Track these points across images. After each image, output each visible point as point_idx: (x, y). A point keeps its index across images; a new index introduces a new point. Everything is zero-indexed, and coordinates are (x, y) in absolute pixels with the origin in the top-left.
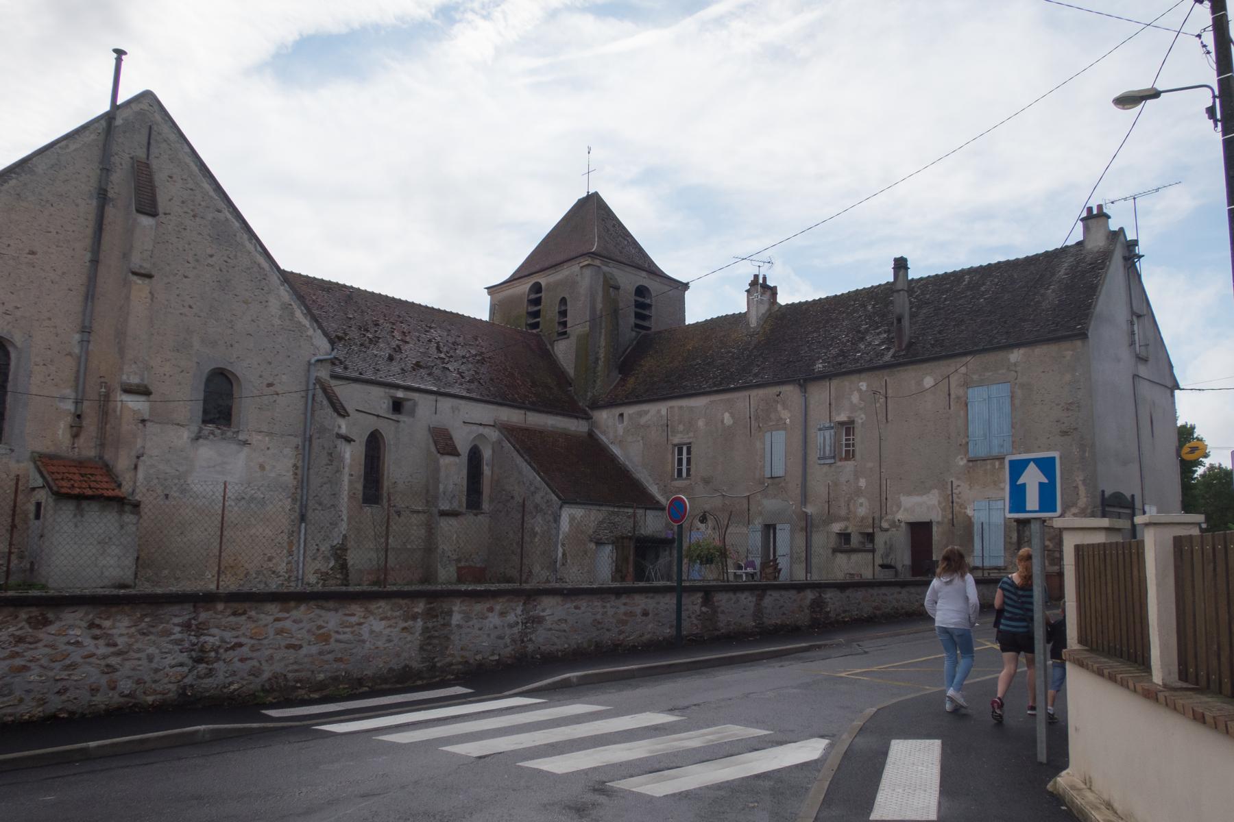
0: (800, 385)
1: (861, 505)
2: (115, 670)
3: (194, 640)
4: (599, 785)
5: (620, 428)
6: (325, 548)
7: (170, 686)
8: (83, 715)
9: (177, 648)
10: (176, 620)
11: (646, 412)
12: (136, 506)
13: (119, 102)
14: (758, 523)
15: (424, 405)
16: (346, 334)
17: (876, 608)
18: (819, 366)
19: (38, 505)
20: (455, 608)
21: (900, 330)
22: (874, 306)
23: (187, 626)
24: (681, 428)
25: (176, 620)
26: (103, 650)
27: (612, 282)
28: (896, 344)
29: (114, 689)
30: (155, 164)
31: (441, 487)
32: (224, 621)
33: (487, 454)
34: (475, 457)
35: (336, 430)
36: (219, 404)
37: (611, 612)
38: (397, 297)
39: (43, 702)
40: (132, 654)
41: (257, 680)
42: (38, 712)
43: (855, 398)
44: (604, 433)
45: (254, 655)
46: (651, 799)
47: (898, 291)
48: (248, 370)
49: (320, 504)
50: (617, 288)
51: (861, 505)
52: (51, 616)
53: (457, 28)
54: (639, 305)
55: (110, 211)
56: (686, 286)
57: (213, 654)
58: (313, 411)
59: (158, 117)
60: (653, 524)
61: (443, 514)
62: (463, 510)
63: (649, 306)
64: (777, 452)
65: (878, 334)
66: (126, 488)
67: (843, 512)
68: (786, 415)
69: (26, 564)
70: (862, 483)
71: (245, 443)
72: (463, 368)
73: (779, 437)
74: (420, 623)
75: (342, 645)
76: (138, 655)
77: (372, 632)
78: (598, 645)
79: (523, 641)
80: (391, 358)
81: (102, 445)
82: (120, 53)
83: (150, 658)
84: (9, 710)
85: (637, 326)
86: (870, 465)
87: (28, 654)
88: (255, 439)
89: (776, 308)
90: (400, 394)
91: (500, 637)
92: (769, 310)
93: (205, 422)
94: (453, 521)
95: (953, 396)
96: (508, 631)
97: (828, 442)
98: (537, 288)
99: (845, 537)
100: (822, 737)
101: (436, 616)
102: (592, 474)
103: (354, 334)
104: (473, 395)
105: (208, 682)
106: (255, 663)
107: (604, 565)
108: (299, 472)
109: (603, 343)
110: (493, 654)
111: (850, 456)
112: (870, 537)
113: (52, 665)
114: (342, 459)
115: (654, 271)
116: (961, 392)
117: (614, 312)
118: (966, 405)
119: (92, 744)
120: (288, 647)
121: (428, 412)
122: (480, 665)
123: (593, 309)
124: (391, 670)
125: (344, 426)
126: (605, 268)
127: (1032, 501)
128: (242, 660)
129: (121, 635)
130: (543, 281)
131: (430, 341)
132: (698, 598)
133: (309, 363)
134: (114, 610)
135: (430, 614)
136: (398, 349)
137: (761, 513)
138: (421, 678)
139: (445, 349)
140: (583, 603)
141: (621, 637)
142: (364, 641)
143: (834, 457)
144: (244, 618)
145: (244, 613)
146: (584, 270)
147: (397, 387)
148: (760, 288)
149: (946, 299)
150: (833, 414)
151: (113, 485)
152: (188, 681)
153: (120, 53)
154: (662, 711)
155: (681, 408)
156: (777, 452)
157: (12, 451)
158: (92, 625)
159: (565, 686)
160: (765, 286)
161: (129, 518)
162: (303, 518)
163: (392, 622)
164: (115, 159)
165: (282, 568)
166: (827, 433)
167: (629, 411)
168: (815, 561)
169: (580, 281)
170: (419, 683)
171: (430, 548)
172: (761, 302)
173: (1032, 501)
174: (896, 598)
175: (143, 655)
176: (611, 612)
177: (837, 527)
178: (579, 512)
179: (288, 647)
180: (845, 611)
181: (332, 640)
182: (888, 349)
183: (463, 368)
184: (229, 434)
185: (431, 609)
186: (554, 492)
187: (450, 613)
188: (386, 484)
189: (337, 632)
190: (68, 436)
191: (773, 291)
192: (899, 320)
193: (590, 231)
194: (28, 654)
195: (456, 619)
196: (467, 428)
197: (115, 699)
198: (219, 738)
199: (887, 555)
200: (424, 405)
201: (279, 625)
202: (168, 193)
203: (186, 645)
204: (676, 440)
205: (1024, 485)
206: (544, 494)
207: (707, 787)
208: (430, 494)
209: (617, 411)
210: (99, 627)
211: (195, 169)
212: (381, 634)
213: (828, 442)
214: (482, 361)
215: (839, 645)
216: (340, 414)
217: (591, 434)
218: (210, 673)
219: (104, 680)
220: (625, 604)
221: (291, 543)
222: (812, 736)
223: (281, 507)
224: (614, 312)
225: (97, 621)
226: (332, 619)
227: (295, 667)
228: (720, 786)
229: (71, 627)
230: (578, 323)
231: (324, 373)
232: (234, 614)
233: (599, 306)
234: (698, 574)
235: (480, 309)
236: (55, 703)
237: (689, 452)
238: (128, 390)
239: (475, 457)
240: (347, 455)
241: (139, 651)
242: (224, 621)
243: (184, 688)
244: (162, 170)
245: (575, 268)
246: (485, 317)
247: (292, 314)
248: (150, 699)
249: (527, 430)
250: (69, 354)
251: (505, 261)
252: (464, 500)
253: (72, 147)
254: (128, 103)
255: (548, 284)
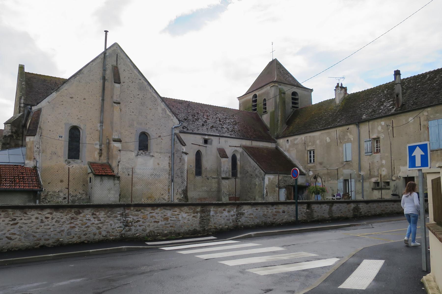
0: (357, 125)
1: (383, 171)
2: (101, 228)
3: (124, 219)
4: (242, 270)
5: (288, 145)
6: (180, 190)
7: (118, 234)
8: (92, 242)
9: (119, 222)
10: (119, 213)
11: (297, 139)
12: (119, 178)
13: (107, 48)
14: (341, 179)
15: (215, 140)
16: (188, 118)
17: (382, 211)
18: (364, 117)
19: (90, 178)
20: (212, 209)
21: (398, 99)
22: (387, 91)
23: (122, 215)
24: (310, 144)
25: (119, 213)
26: (97, 222)
27: (282, 91)
28: (396, 105)
29: (100, 234)
30: (119, 66)
31: (222, 169)
32: (133, 213)
33: (238, 157)
34: (234, 158)
35: (182, 150)
36: (144, 143)
37: (270, 211)
38: (205, 104)
39: (80, 238)
40: (105, 223)
41: (145, 233)
42: (79, 240)
43: (380, 128)
44: (281, 147)
45: (144, 224)
46: (258, 276)
47: (396, 84)
48: (152, 132)
49: (178, 176)
50: (284, 93)
51: (383, 171)
52: (81, 211)
53: (230, 6)
54: (293, 99)
55: (106, 83)
56: (312, 90)
57: (130, 224)
58: (174, 144)
59: (119, 51)
60: (301, 180)
61: (223, 178)
62: (231, 177)
63: (297, 99)
64: (348, 151)
65: (389, 102)
66: (116, 172)
67: (376, 174)
68: (351, 137)
69: (88, 197)
70: (384, 162)
71: (153, 156)
72: (229, 127)
73: (349, 145)
74: (199, 214)
75: (173, 222)
76: (107, 224)
77: (182, 217)
78: (265, 223)
79: (236, 221)
80: (203, 125)
81: (108, 159)
82: (106, 32)
83: (111, 225)
84: (70, 240)
85: (293, 107)
86: (386, 155)
87: (75, 223)
88: (156, 155)
89: (347, 95)
90: (207, 137)
91: (228, 220)
92: (344, 96)
93: (139, 150)
94: (227, 181)
95: (422, 125)
96: (231, 218)
97: (369, 146)
98: (255, 96)
99: (377, 183)
100: (337, 258)
101: (205, 212)
102: (278, 163)
103: (190, 117)
104: (232, 136)
105: (129, 233)
106: (144, 227)
107: (283, 195)
108: (171, 165)
109: (280, 114)
110: (226, 226)
111: (378, 151)
112: (388, 183)
113: (82, 226)
114: (184, 160)
115: (299, 86)
116: (425, 123)
117: (283, 102)
118: (428, 128)
119: (91, 251)
120: (155, 222)
121: (217, 143)
122: (221, 229)
123: (276, 102)
124: (189, 230)
125: (184, 149)
126: (280, 87)
127: (418, 162)
128: (140, 226)
129: (102, 217)
130: (257, 93)
131: (217, 118)
132: (305, 206)
133: (172, 128)
134: (99, 209)
135: (202, 211)
136: (206, 122)
137: (342, 175)
138: (200, 234)
139: (222, 120)
140: (259, 208)
141: (274, 220)
142: (180, 220)
143: (371, 152)
144: (140, 212)
145: (140, 210)
146: (272, 88)
147: (205, 135)
148: (340, 88)
149: (418, 86)
150: (371, 135)
151: (112, 171)
152: (123, 232)
153: (106, 32)
154: (280, 247)
155: (310, 136)
156: (348, 151)
157: (82, 161)
158: (93, 214)
159: (249, 237)
160: (342, 87)
161: (117, 182)
162: (172, 181)
163: (189, 214)
164: (107, 66)
165: (166, 197)
166: (368, 143)
167: (290, 139)
168: (365, 193)
169: (271, 91)
170: (199, 235)
171: (219, 190)
172: (340, 93)
173: (418, 162)
174: (390, 207)
175: (109, 224)
176: (270, 211)
177: (373, 180)
178: (272, 177)
179: (155, 222)
180: (369, 212)
181: (169, 220)
182: (393, 108)
183: (229, 127)
184: (147, 153)
185: (203, 210)
186: (262, 170)
187: (210, 211)
188: (203, 169)
189: (171, 217)
190: (98, 156)
191: (345, 89)
192: (397, 96)
193: (275, 73)
194: (75, 223)
195: (212, 213)
196: (231, 148)
197: (101, 238)
198: (129, 250)
199: (395, 190)
200: (215, 140)
201: (151, 214)
202: (123, 76)
203: (122, 220)
204: (309, 149)
205: (415, 156)
206: (259, 170)
207: (282, 273)
208: (218, 171)
209: (286, 139)
210: (95, 214)
211: (132, 67)
212: (186, 218)
213: (369, 146)
214: (235, 124)
215: (363, 225)
216: (183, 145)
217: (277, 148)
218: (130, 230)
219: (97, 231)
220: (275, 208)
221: (169, 189)
222: (334, 257)
223: (165, 177)
224: (283, 102)
225: (95, 213)
226: (169, 213)
227: (157, 229)
228: (287, 273)
229: (87, 214)
230: (270, 108)
231: (177, 131)
232: (137, 211)
233: (278, 100)
234: (314, 198)
235: (236, 106)
236: (83, 238)
237: (314, 153)
238: (115, 141)
239: (234, 158)
240: (186, 159)
241: (107, 222)
242: (133, 213)
243: (122, 235)
244: (121, 68)
245: (268, 88)
246: (237, 108)
247: (166, 112)
248: (111, 238)
249: (252, 147)
250: (97, 130)
251: (243, 88)
252: (231, 174)
253: (94, 64)
254: (110, 47)
255: (259, 95)
